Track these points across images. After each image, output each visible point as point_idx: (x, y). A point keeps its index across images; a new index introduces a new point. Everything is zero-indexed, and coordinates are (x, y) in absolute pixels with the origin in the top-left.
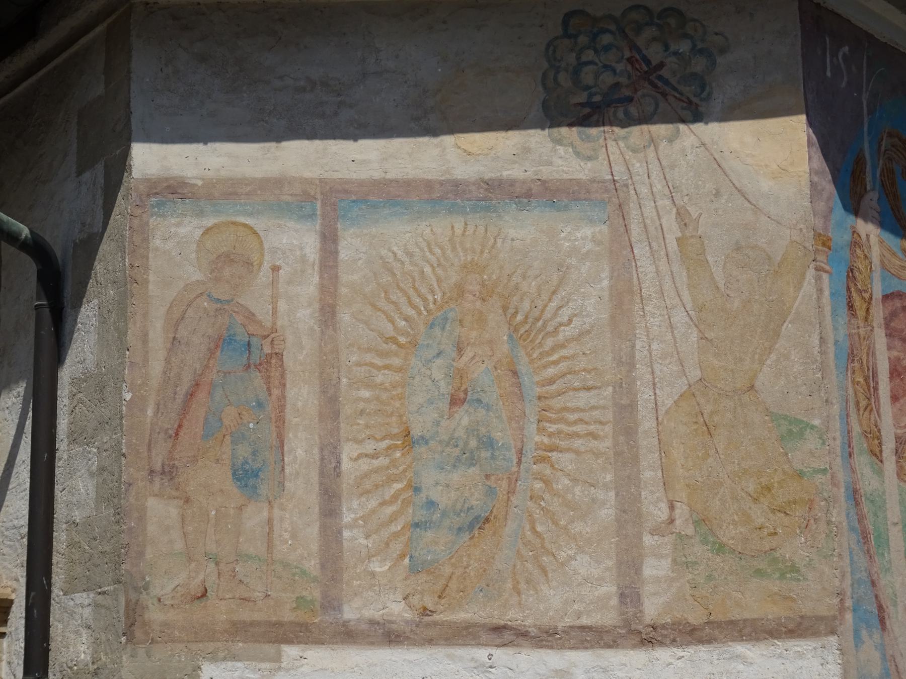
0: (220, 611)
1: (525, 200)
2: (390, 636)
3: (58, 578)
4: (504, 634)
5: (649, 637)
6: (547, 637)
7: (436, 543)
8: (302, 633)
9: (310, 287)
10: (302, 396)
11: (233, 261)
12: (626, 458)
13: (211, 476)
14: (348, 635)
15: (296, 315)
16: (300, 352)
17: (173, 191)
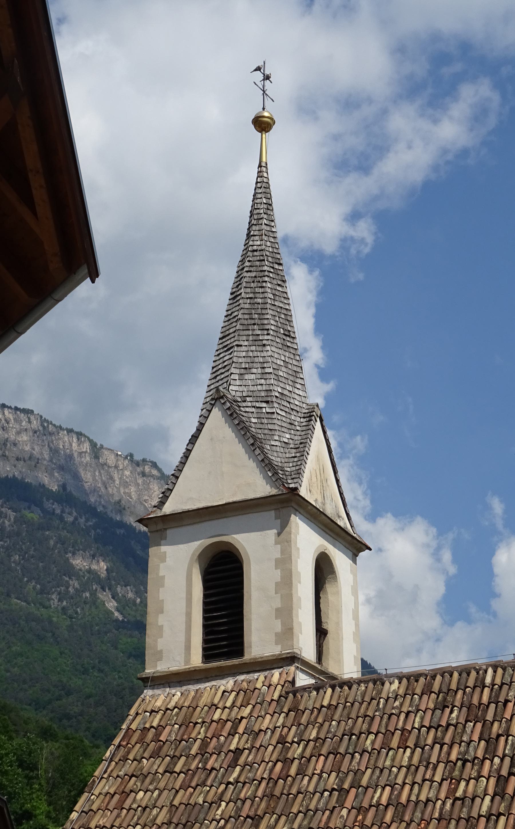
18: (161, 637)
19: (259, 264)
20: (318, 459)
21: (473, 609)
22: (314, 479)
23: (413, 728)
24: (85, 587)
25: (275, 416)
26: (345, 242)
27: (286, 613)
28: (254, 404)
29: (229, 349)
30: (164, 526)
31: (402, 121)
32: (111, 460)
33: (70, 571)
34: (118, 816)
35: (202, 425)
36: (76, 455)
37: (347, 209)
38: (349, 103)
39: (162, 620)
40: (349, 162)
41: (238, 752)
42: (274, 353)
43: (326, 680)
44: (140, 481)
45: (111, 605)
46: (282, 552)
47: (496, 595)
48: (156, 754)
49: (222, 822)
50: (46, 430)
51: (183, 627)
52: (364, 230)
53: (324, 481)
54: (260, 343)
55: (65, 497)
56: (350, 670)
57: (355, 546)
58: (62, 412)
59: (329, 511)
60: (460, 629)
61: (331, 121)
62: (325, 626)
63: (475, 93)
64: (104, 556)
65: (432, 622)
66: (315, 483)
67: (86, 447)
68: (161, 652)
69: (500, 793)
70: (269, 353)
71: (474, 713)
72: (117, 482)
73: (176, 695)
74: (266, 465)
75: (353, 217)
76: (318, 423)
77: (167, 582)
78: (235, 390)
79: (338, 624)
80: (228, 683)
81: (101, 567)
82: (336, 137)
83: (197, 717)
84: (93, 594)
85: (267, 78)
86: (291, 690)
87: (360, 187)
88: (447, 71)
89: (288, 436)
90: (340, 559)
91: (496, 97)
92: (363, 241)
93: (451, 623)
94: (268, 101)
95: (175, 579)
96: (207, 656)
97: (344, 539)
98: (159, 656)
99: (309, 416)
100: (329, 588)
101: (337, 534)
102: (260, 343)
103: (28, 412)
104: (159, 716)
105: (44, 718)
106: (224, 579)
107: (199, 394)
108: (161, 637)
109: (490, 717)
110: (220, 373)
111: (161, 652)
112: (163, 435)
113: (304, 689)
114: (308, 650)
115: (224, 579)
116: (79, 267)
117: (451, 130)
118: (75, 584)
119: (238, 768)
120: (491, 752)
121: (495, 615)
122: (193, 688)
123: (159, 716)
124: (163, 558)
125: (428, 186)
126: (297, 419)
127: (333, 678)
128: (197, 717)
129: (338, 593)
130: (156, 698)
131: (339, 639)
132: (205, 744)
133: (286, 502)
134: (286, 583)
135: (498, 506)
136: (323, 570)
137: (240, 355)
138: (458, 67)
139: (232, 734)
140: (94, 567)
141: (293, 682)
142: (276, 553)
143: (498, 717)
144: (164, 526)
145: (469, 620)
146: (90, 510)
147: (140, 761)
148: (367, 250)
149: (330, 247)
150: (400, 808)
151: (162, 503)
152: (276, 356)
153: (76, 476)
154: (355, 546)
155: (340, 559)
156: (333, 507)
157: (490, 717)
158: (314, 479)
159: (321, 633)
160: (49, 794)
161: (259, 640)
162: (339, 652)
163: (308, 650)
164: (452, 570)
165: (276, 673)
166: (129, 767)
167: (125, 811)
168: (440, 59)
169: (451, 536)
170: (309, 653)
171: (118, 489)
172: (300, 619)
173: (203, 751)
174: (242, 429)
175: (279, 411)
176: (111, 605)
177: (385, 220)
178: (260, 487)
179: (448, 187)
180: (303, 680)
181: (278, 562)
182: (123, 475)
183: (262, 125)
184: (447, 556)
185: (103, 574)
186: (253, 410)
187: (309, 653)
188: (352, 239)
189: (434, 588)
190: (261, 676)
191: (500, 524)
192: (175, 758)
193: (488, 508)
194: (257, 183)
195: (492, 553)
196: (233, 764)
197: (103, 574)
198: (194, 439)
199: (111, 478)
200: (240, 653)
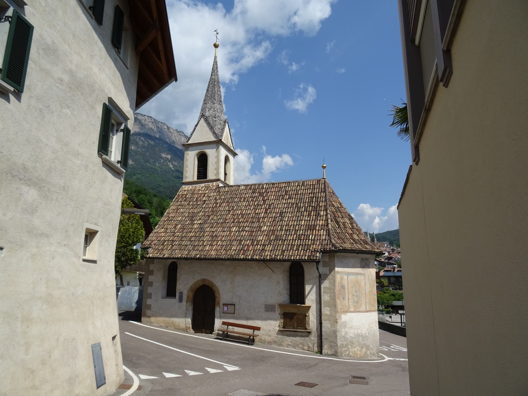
0: (342, 310)
1: (312, 257)
2: (353, 312)
3: (322, 305)
4: (359, 312)
5: (367, 312)
6: (362, 312)
7: (355, 304)
8: (347, 312)
9: (346, 282)
10: (346, 291)
11: (342, 279)
12: (366, 297)
13: (341, 298)
14: (350, 312)
15: (346, 283)
16: (346, 288)
17: (338, 272)
19: (214, 82)
21: (257, 172)
24: (165, 161)
26: (231, 81)
27: (217, 169)
29: (206, 104)
30: (188, 146)
31: (247, 50)
32: (172, 131)
33: (161, 157)
35: (198, 122)
37: (232, 72)
38: (234, 44)
39: (187, 169)
40: (234, 60)
41: (205, 201)
42: (217, 105)
43: (226, 185)
45: (171, 166)
47: (263, 169)
48: (185, 201)
50: (155, 122)
51: (192, 171)
52: (236, 78)
53: (228, 138)
55: (160, 139)
56: (231, 183)
57: (234, 154)
58: (160, 118)
59: (229, 146)
60: (254, 177)
61: (229, 49)
63: (266, 44)
64: (170, 154)
65: (248, 174)
66: (226, 138)
67: (166, 127)
69: (266, 212)
71: (261, 194)
73: (190, 187)
74: (214, 133)
75: (233, 74)
77: (189, 160)
78: (207, 114)
79: (230, 172)
80: (203, 185)
81: (169, 157)
82: (230, 53)
83: (195, 192)
84: (167, 163)
85: (218, 33)
86: (218, 187)
87: (236, 67)
88: (259, 38)
90: (231, 157)
91: (270, 47)
92: (235, 81)
93: (252, 175)
95: (191, 160)
96: (198, 178)
98: (186, 178)
99: (225, 122)
100: (228, 164)
103: (151, 117)
105: (154, 192)
106: (203, 159)
107: (198, 114)
109: (264, 195)
110: (203, 109)
112: (185, 126)
113: (221, 187)
114: (222, 178)
115: (203, 159)
116: (172, 78)
117: (259, 54)
118: (162, 160)
120: (264, 203)
121: (262, 174)
122: (194, 186)
124: (188, 154)
125: (252, 67)
126: (222, 122)
127: (228, 185)
128: (195, 192)
129: (230, 165)
130: (186, 187)
131: (230, 176)
132: (197, 199)
133: (218, 142)
134: (218, 162)
135: (264, 148)
136: (227, 159)
137: (208, 105)
138: (261, 37)
139: (204, 197)
142: (216, 154)
143: (266, 196)
144: (188, 146)
145: (256, 174)
146: (167, 143)
148: (236, 83)
149: (227, 81)
150: (243, 215)
151: (188, 141)
154: (234, 154)
155: (231, 157)
156: (230, 144)
157: (264, 195)
159: (226, 174)
160: (156, 210)
161: (211, 175)
162: (229, 179)
164: (253, 162)
165: (215, 183)
166: (179, 203)
168: (257, 35)
169: (253, 154)
170: (222, 179)
173: (197, 200)
174: (208, 124)
176: (171, 166)
177: (241, 76)
178: (212, 139)
179: (257, 69)
180: (221, 185)
181: (216, 157)
183: (216, 46)
184: (252, 159)
185: (169, 159)
187: (222, 179)
188: (233, 80)
189: (248, 167)
190: (211, 184)
191: (264, 152)
192: (190, 202)
193: (262, 148)
195: (263, 159)
196: (204, 204)
197: (169, 159)
198: (196, 126)
200: (206, 178)
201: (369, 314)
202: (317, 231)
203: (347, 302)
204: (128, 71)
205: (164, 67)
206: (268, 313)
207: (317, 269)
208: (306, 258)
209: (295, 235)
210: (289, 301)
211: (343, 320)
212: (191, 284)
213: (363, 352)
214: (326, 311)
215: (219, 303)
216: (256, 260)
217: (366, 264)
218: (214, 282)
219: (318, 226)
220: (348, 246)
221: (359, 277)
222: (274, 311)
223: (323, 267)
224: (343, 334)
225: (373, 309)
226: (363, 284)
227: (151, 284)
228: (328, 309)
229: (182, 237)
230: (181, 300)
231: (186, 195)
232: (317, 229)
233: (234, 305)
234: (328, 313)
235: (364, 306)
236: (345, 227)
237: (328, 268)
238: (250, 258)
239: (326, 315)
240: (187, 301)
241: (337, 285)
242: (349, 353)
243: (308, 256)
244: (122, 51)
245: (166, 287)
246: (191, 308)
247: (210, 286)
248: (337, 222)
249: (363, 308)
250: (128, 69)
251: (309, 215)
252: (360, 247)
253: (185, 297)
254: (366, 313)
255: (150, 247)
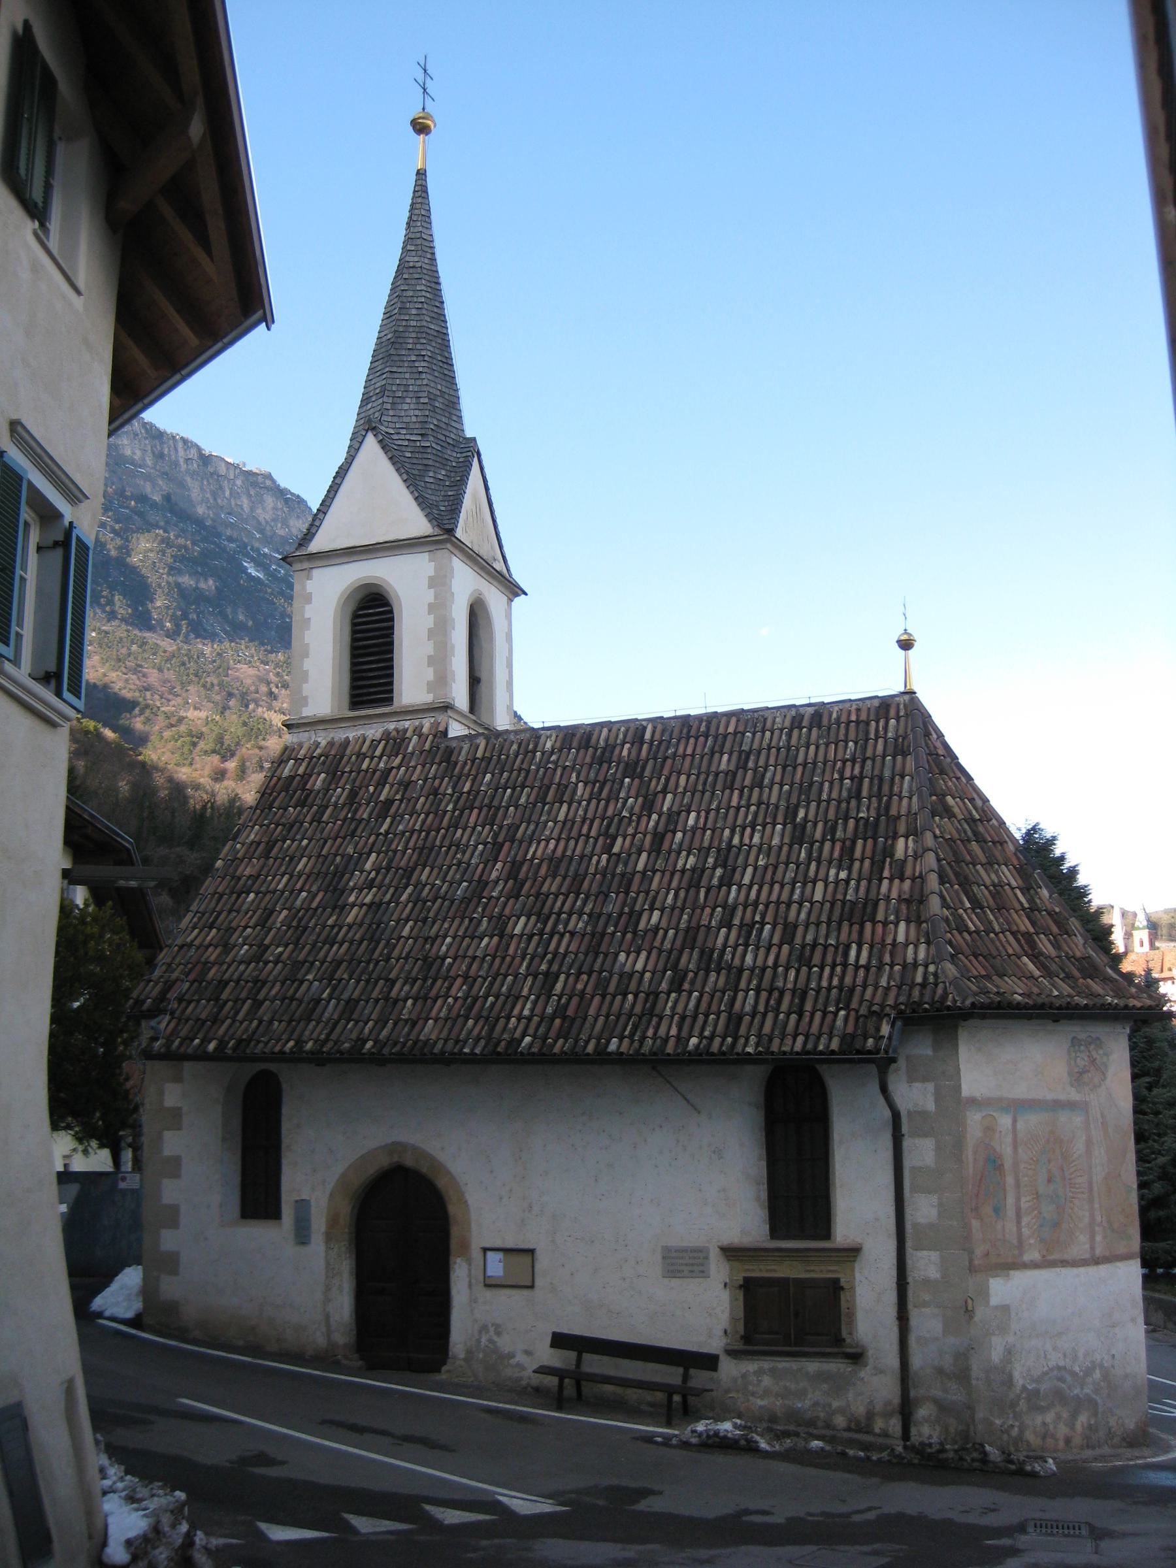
2: (1035, 1265)
3: (909, 1244)
4: (1064, 1263)
5: (1096, 1261)
6: (1074, 1264)
10: (1010, 1180)
12: (1091, 1201)
14: (1025, 1266)
15: (1007, 1151)
18: (307, 682)
20: (475, 498)
22: (470, 519)
23: (570, 783)
25: (429, 450)
27: (439, 660)
28: (408, 437)
34: (264, 865)
36: (181, 461)
41: (389, 802)
44: (252, 492)
46: (436, 597)
49: (373, 873)
54: (415, 370)
59: (483, 553)
62: (477, 674)
68: (306, 698)
70: (425, 382)
72: (227, 493)
76: (476, 459)
89: (443, 472)
90: (494, 598)
94: (428, 101)
97: (500, 582)
101: (494, 578)
102: (415, 370)
104: (304, 764)
108: (307, 682)
111: (306, 698)
119: (388, 820)
123: (304, 764)
140: (202, 585)
141: (445, 733)
147: (286, 810)
152: (432, 384)
153: (182, 484)
158: (470, 519)
159: (474, 681)
163: (460, 696)
167: (272, 860)
171: (229, 500)
172: (454, 668)
175: (434, 445)
182: (234, 484)
186: (406, 443)
194: (415, 191)
199: (221, 488)
200: (389, 700)
201: (1103, 1270)
202: (879, 927)
203: (1011, 1226)
204: (77, 302)
205: (213, 271)
206: (675, 1282)
207: (884, 1089)
208: (835, 1044)
209: (786, 948)
210: (767, 1228)
211: (994, 1301)
212: (340, 1168)
213: (1079, 1427)
214: (926, 1264)
215: (465, 1247)
216: (619, 1059)
217: (1093, 1061)
218: (442, 1157)
219: (882, 905)
220: (1016, 990)
221: (1063, 1117)
222: (704, 1274)
223: (911, 1080)
224: (996, 1355)
225: (1121, 1249)
226: (1079, 1147)
227: (173, 1167)
228: (934, 1256)
229: (297, 965)
230: (302, 1236)
231: (306, 776)
232: (880, 916)
233: (531, 1252)
234: (933, 1273)
235: (1083, 1238)
236: (1001, 907)
237: (930, 1087)
238: (590, 1048)
239: (927, 1282)
240: (329, 1237)
241: (969, 1154)
242: (1021, 1432)
243: (843, 1038)
244: (54, 225)
245: (237, 1180)
246: (346, 1268)
247: (424, 1170)
248: (966, 884)
249: (1080, 1247)
250: (78, 293)
251: (848, 852)
252: (1066, 989)
253: (319, 1224)
254: (1092, 1270)
255: (163, 1012)
